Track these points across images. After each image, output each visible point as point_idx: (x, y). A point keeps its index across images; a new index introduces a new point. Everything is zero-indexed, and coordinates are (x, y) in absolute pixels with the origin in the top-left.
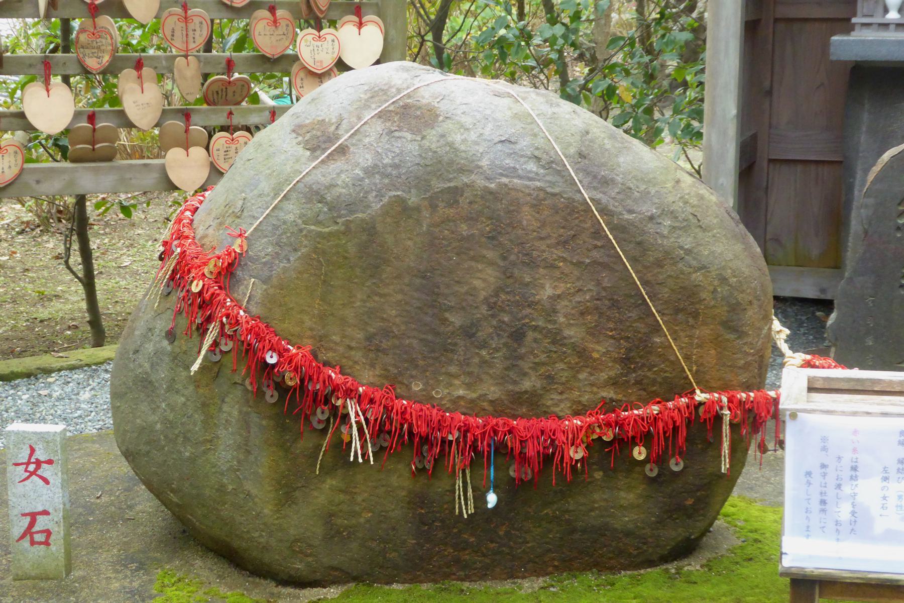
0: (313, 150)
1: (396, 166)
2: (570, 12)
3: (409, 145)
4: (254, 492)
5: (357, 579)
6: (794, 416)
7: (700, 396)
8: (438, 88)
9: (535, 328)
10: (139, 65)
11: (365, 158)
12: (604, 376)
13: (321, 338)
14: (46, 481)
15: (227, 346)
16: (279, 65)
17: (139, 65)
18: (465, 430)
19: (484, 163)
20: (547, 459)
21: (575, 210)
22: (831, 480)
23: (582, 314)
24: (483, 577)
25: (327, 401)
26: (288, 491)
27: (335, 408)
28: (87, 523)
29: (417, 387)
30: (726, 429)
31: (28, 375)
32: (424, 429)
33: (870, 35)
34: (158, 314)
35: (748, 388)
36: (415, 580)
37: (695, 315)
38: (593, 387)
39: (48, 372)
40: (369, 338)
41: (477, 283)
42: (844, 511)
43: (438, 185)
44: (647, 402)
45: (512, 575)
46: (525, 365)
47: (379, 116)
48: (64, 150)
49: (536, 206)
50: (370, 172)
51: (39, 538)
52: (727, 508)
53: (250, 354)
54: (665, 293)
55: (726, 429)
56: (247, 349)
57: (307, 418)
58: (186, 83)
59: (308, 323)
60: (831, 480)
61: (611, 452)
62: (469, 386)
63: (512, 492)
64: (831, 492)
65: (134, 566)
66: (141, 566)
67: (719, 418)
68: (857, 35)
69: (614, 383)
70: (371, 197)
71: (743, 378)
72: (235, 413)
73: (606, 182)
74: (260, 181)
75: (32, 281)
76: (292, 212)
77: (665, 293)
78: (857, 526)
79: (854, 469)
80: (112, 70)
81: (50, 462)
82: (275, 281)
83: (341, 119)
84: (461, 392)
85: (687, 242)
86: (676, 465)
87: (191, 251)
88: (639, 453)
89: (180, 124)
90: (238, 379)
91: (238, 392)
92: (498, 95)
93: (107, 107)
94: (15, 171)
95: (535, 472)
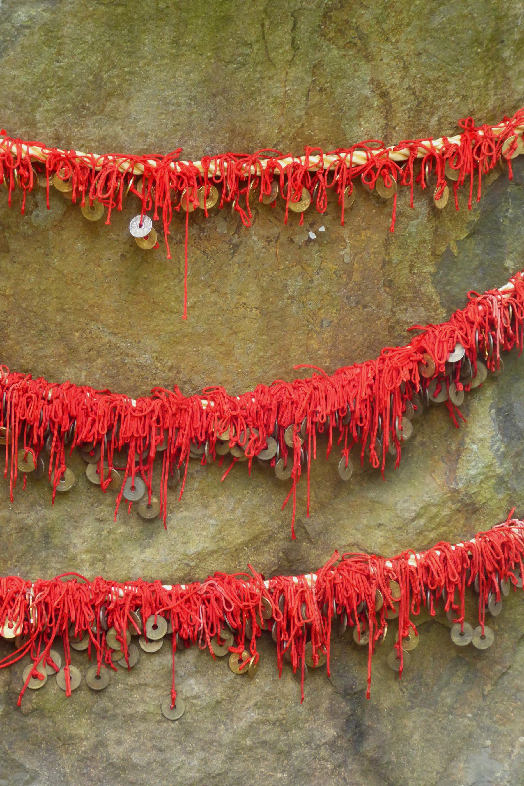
30: (53, 637)
55: (53, 637)
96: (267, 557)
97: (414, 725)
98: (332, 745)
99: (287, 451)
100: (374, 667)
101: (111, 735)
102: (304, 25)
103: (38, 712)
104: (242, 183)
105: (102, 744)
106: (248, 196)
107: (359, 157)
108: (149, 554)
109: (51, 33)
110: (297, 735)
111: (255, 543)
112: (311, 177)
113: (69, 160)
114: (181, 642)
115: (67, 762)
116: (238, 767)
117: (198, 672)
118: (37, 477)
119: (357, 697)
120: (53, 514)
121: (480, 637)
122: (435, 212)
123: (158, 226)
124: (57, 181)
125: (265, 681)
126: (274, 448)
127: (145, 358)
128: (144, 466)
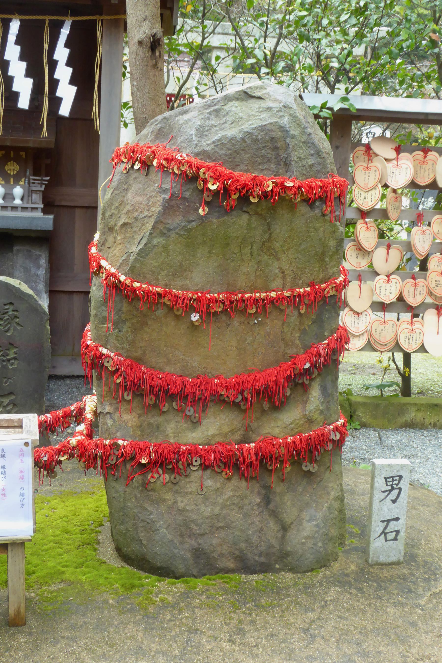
96: (237, 436)
97: (288, 498)
98: (258, 505)
100: (274, 478)
101: (179, 499)
103: (153, 490)
104: (231, 302)
105: (176, 502)
106: (234, 307)
107: (274, 294)
108: (194, 435)
109: (165, 248)
110: (246, 501)
111: (232, 432)
112: (256, 301)
113: (170, 293)
114: (205, 467)
115: (163, 508)
116: (224, 512)
117: (211, 478)
118: (155, 406)
119: (268, 488)
120: (160, 419)
122: (300, 315)
123: (201, 317)
124: (166, 300)
125: (235, 482)
126: (240, 398)
127: (195, 364)
128: (194, 403)
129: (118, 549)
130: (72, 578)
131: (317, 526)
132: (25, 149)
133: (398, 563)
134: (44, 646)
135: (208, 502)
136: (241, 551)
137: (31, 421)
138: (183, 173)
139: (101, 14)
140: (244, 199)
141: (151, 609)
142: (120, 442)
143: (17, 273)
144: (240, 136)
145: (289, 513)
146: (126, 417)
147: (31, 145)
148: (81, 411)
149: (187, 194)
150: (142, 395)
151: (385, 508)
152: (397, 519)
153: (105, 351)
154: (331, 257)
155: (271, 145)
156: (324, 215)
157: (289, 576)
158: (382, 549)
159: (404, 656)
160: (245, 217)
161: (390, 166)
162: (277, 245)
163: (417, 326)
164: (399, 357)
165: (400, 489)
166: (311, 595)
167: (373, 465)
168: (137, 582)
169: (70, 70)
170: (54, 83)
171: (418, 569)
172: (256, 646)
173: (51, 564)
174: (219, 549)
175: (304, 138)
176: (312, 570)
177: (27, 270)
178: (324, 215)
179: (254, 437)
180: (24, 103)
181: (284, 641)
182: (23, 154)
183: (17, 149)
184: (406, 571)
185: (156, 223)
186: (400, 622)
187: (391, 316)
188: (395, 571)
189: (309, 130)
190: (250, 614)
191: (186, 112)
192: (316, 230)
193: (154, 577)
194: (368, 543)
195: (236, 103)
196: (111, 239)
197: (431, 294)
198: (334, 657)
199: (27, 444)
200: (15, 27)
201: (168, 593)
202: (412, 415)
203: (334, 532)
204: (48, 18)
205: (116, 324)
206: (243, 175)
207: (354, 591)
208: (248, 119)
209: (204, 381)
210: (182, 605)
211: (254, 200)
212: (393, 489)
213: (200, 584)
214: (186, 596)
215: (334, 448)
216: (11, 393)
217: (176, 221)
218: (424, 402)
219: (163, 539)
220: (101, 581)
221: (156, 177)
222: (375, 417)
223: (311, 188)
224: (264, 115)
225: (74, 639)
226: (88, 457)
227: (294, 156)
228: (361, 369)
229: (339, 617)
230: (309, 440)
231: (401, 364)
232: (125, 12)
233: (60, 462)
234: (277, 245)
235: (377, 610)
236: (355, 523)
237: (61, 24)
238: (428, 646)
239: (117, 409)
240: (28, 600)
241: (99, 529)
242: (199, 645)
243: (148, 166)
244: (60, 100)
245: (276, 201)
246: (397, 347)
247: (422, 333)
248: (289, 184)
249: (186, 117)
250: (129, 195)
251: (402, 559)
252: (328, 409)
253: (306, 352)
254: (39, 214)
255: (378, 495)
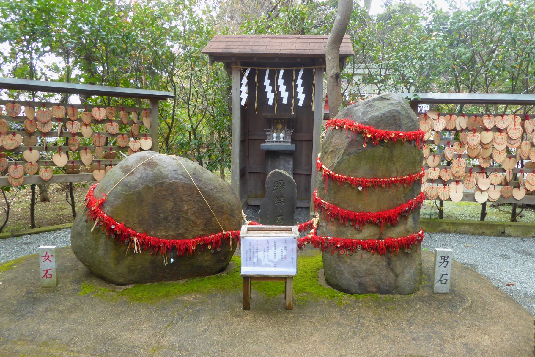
0: (125, 173)
1: (146, 177)
2: (199, 137)
3: (150, 172)
4: (109, 261)
5: (137, 283)
6: (243, 237)
7: (224, 232)
8: (158, 158)
9: (183, 217)
10: (86, 149)
11: (138, 175)
12: (200, 228)
13: (127, 221)
14: (51, 261)
15: (101, 224)
16: (125, 149)
17: (86, 149)
18: (165, 243)
19: (169, 176)
20: (186, 250)
21: (192, 188)
22: (252, 252)
23: (195, 213)
24: (170, 280)
25: (128, 237)
26: (118, 261)
27: (130, 239)
28: (64, 271)
29: (152, 233)
30: (231, 240)
31: (54, 230)
32: (154, 244)
33: (269, 144)
34: (83, 216)
35: (236, 230)
36: (152, 282)
37: (223, 213)
38: (198, 231)
39: (60, 229)
40: (139, 221)
41: (168, 206)
42: (255, 260)
43: (157, 182)
44: (211, 234)
45: (178, 279)
46: (180, 227)
47: (142, 164)
48: (65, 170)
49: (183, 187)
50: (140, 178)
51: (48, 276)
52: (233, 258)
53: (108, 226)
54: (215, 208)
55: (231, 240)
56: (106, 225)
57: (123, 242)
58: (100, 153)
59: (123, 217)
60: (252, 252)
61: (202, 247)
62: (166, 232)
63: (176, 258)
64: (252, 255)
65: (76, 282)
66: (78, 282)
67: (229, 238)
68: (267, 144)
69: (203, 230)
70: (140, 185)
71: (235, 228)
72: (104, 241)
73: (200, 181)
74: (109, 181)
75: (59, 204)
76: (119, 189)
77: (215, 208)
78: (258, 263)
79: (257, 250)
80: (79, 149)
81: (52, 256)
82: (114, 207)
83: (132, 165)
84: (164, 234)
85: (220, 195)
86: (219, 250)
87: (92, 199)
88: (209, 247)
89: (97, 164)
90: (104, 232)
91: (104, 236)
92: (173, 159)
93: (78, 159)
94: (51, 176)
95: (183, 253)
96: (377, 237)
97: (398, 263)
98: (385, 266)
99: (380, 222)
100: (392, 255)
101: (353, 262)
102: (386, 160)
103: (342, 258)
104: (375, 182)
105: (351, 263)
106: (377, 184)
107: (393, 179)
108: (359, 236)
109: (349, 160)
110: (380, 264)
111: (375, 235)
112: (386, 181)
113: (350, 178)
114: (363, 249)
115: (346, 265)
116: (371, 268)
117: (366, 253)
118: (343, 224)
119: (389, 259)
120: (345, 229)
121: (409, 251)
122: (404, 187)
123: (363, 188)
124: (348, 181)
125: (376, 255)
126: (378, 221)
127: (359, 207)
128: (359, 223)
129: (327, 281)
130: (309, 291)
131: (411, 275)
132: (284, 119)
133: (447, 294)
134: (300, 319)
135: (365, 263)
136: (378, 284)
137: (295, 228)
138: (357, 131)
139: (315, 65)
140: (382, 141)
141: (342, 306)
142: (329, 238)
143: (281, 167)
144: (380, 115)
145: (398, 270)
146: (332, 228)
147: (287, 117)
148: (312, 224)
149: (358, 139)
150: (338, 219)
151: (441, 270)
152: (446, 274)
153: (323, 201)
154: (418, 163)
155: (393, 118)
156: (415, 146)
157: (399, 296)
158: (438, 286)
159: (453, 335)
160: (382, 148)
161: (435, 122)
162: (395, 159)
163: (447, 189)
164: (438, 202)
165: (448, 262)
166: (409, 305)
167: (436, 251)
168: (335, 295)
169: (303, 88)
170: (297, 93)
171: (456, 296)
172: (387, 325)
173: (300, 285)
174: (369, 283)
175: (407, 115)
176: (409, 294)
177: (285, 166)
178: (415, 146)
179: (384, 237)
180: (285, 101)
181: (399, 324)
182: (283, 121)
183: (281, 119)
184: (450, 297)
185: (345, 150)
186: (450, 320)
187: (435, 185)
188: (446, 297)
189: (409, 112)
190: (384, 312)
191: (357, 106)
192: (412, 153)
193: (342, 293)
194: (433, 284)
195: (378, 102)
196: (326, 157)
197: (453, 175)
198: (422, 333)
199: (295, 238)
200: (282, 72)
201: (349, 300)
202: (444, 227)
203: (418, 278)
204: (294, 68)
205: (328, 190)
206: (382, 131)
207: (428, 305)
208: (384, 108)
209: (363, 214)
210: (355, 305)
211: (386, 141)
212: (444, 261)
213: (361, 297)
214: (356, 302)
215: (418, 243)
216: (281, 215)
217: (353, 150)
218: (450, 221)
219: (346, 277)
220: (321, 293)
221: (345, 133)
222: (428, 227)
223: (410, 135)
224: (390, 106)
225: (312, 317)
226: (315, 243)
227: (403, 122)
228: (427, 208)
229: (422, 315)
230: (407, 239)
231: (439, 206)
232: (325, 64)
233: (304, 244)
234: (395, 159)
235: (439, 314)
236: (425, 275)
237: (299, 71)
238: (464, 331)
239: (327, 224)
240: (293, 299)
241: (318, 271)
242: (363, 323)
243: (342, 128)
244: (299, 100)
245: (397, 141)
246: (438, 198)
247: (449, 192)
248: (401, 134)
249: (357, 108)
250: (334, 139)
251: (448, 292)
252: (416, 226)
253: (406, 203)
254: (290, 144)
255: (438, 264)
